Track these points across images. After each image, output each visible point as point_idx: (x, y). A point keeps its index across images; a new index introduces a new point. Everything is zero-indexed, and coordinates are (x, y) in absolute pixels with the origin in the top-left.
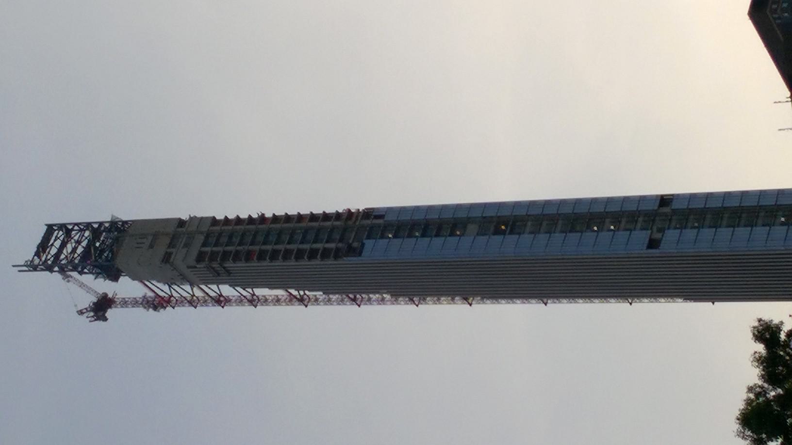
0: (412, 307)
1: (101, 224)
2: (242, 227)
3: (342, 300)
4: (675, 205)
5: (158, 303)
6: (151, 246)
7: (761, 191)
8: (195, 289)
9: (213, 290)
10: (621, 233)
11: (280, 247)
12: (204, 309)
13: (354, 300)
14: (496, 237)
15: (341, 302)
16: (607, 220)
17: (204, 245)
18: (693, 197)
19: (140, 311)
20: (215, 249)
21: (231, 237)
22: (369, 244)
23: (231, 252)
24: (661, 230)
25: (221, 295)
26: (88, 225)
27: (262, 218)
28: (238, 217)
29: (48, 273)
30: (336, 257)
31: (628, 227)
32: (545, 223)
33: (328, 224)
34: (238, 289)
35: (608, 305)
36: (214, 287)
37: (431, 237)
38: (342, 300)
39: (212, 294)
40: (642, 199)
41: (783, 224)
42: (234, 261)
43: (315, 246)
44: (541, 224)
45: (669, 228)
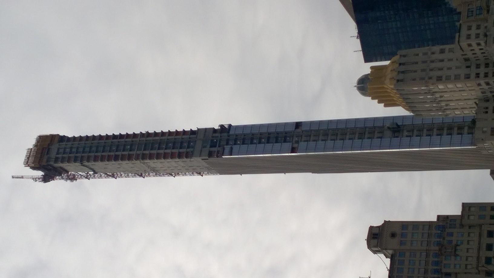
2: (173, 137)
3: (156, 175)
4: (304, 128)
7: (285, 123)
10: (338, 141)
11: (112, 154)
14: (286, 144)
17: (58, 154)
20: (109, 154)
21: (118, 146)
23: (184, 152)
24: (297, 142)
28: (147, 132)
31: (323, 139)
33: (157, 138)
37: (281, 142)
40: (286, 124)
42: (62, 162)
43: (117, 153)
45: (301, 141)
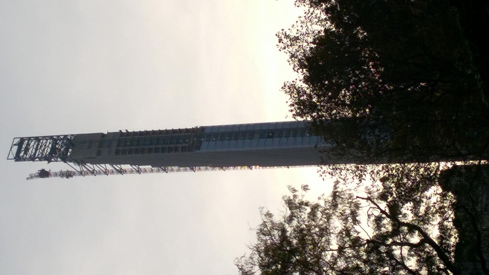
0: (222, 171)
1: (58, 136)
5: (68, 175)
6: (89, 147)
8: (83, 167)
9: (118, 167)
11: (160, 146)
12: (113, 175)
13: (165, 170)
14: (269, 139)
15: (179, 170)
16: (306, 131)
17: (118, 146)
18: (213, 127)
19: (59, 179)
22: (205, 144)
25: (121, 169)
26: (51, 137)
27: (128, 133)
29: (32, 162)
30: (169, 151)
32: (291, 133)
34: (134, 166)
35: (170, 174)
36: (119, 166)
38: (159, 170)
39: (118, 168)
41: (228, 140)
44: (290, 133)
